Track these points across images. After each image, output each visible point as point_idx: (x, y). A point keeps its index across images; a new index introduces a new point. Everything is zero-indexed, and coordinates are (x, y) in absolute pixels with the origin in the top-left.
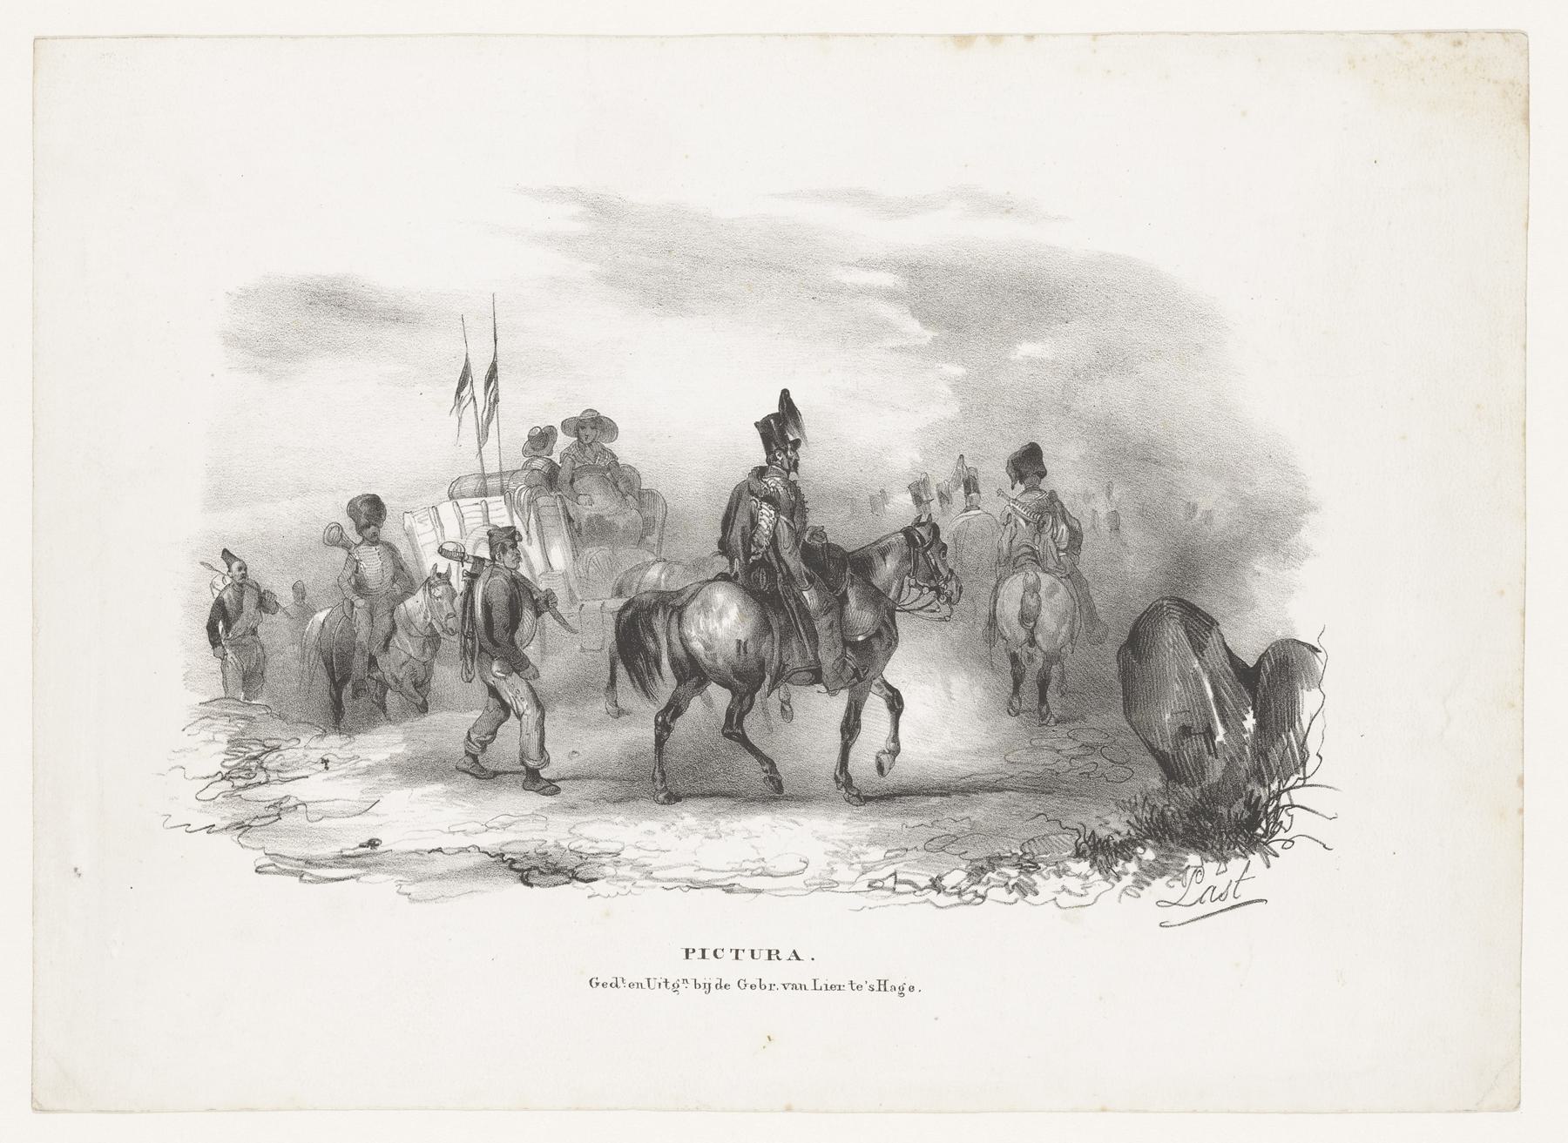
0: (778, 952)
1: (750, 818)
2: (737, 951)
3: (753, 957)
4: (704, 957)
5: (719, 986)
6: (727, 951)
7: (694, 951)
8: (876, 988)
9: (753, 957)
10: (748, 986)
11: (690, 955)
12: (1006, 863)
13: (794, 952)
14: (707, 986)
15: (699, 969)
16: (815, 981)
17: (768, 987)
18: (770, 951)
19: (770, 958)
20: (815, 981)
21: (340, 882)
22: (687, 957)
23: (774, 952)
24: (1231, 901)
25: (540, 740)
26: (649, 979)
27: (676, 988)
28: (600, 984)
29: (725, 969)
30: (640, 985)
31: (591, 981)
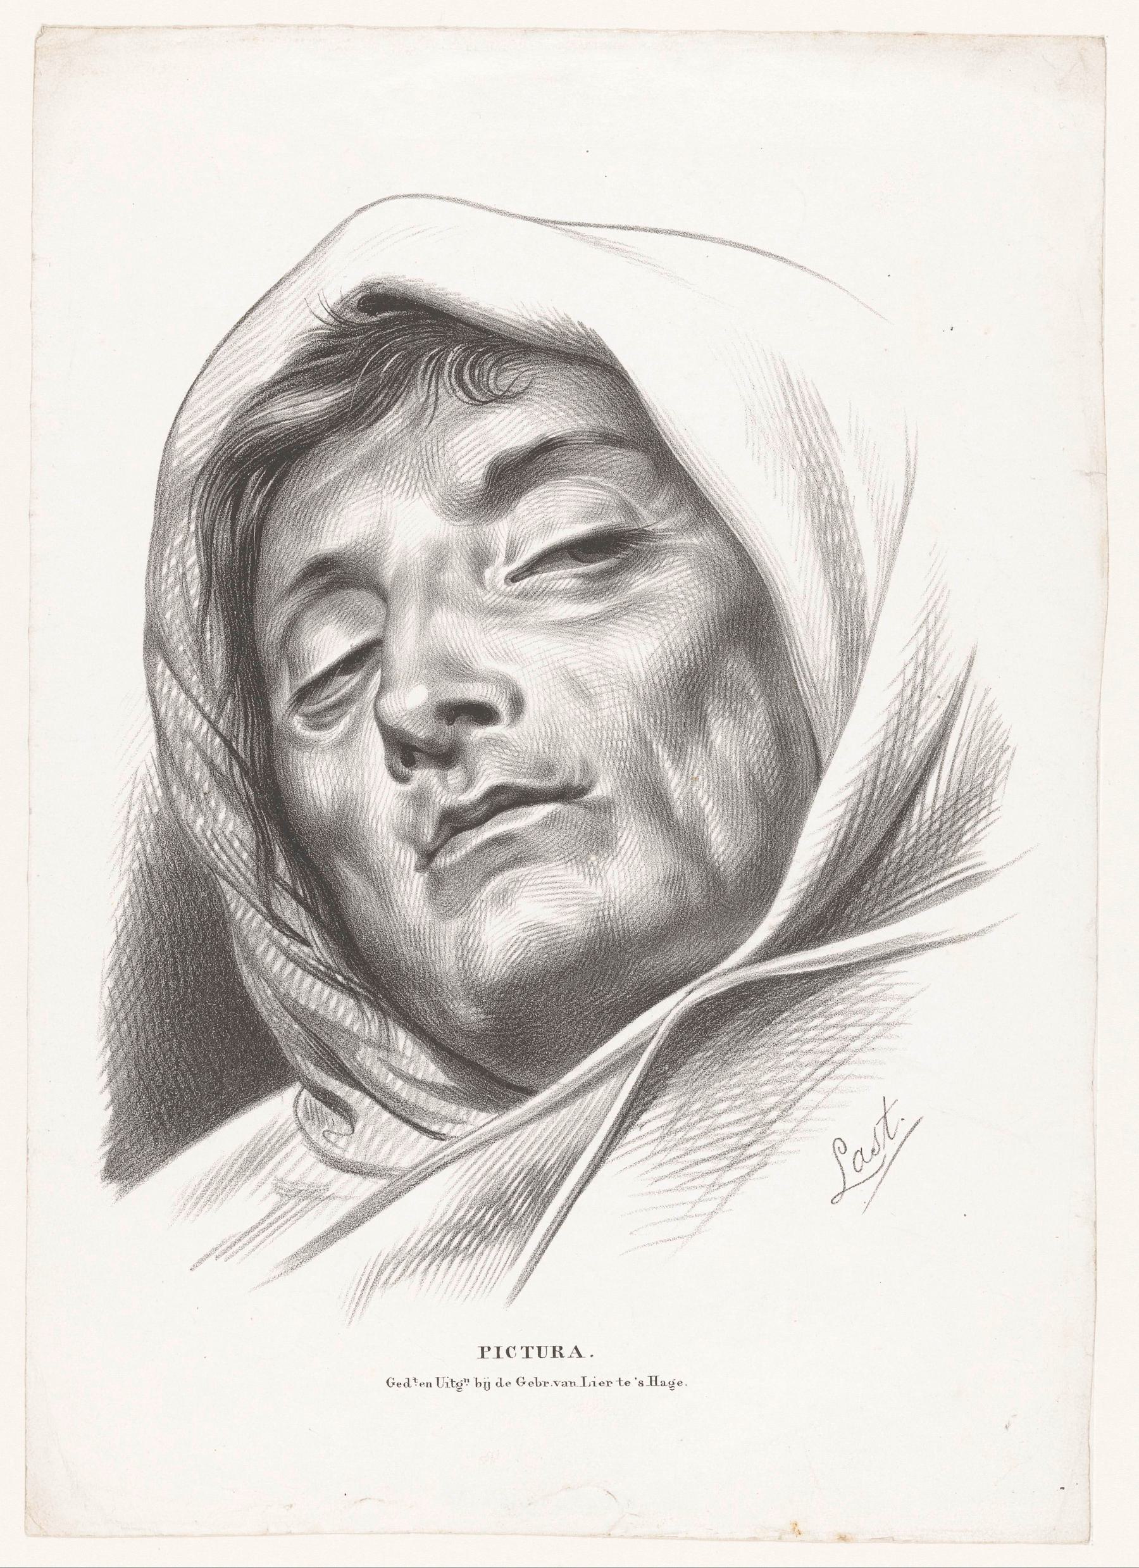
0: (561, 1348)
1: (385, 275)
2: (527, 1348)
4: (498, 1357)
7: (489, 1349)
10: (527, 1383)
13: (576, 1348)
15: (491, 1369)
16: (584, 1378)
17: (543, 1384)
18: (554, 1348)
19: (554, 1356)
20: (584, 1378)
22: (483, 1356)
23: (558, 1349)
26: (438, 1378)
28: (527, 1383)
29: (516, 1366)
30: (429, 1385)
31: (388, 1382)
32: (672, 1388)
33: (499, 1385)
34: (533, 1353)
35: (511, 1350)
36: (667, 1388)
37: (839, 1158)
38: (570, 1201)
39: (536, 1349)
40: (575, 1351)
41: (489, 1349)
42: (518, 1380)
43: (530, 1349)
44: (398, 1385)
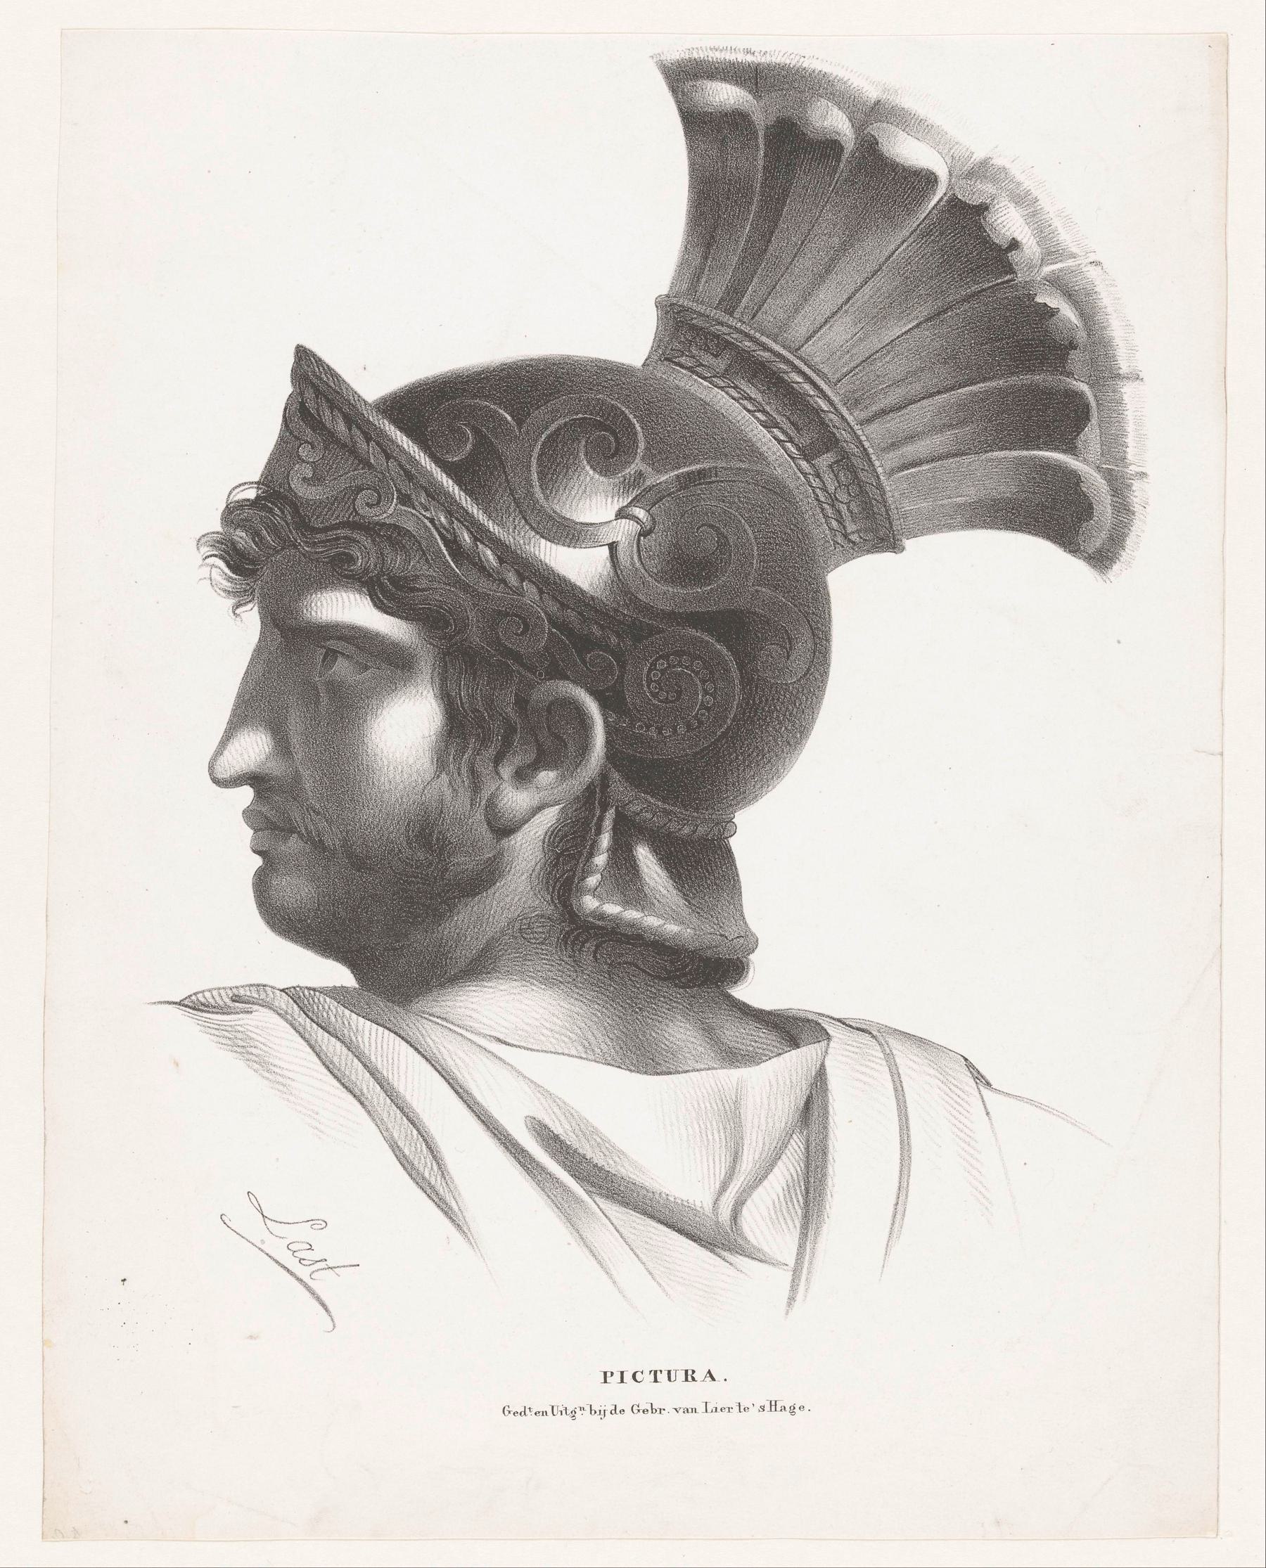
3: (669, 1379)
4: (622, 1381)
6: (646, 1372)
9: (669, 1379)
10: (641, 1411)
11: (608, 1379)
12: (659, 313)
13: (709, 1372)
14: (602, 1412)
15: (618, 1394)
18: (686, 1371)
21: (237, 484)
22: (605, 1382)
23: (690, 1373)
24: (303, 1272)
26: (553, 1407)
27: (573, 1415)
28: (641, 1411)
32: (792, 1412)
33: (523, 1413)
34: (662, 1377)
36: (787, 1413)
37: (982, 1093)
38: (440, 1069)
39: (665, 1373)
40: (708, 1375)
42: (504, 1408)
43: (659, 1372)
44: (644, 1411)
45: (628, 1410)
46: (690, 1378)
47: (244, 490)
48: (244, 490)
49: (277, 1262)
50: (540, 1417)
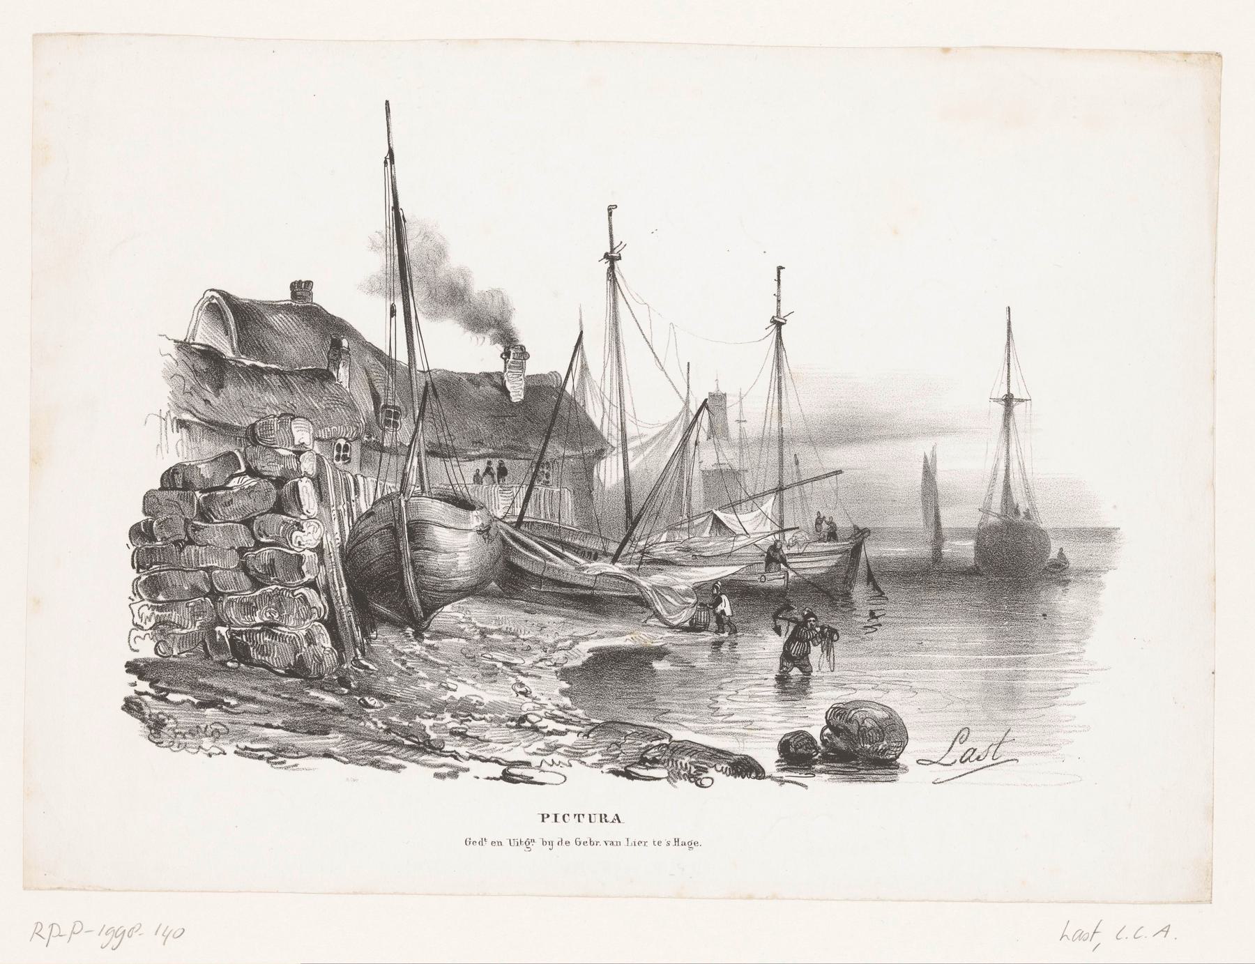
0: (606, 816)
2: (579, 815)
4: (556, 821)
5: (560, 843)
8: (581, 816)
11: (545, 819)
15: (552, 830)
18: (601, 815)
19: (601, 821)
22: (543, 821)
23: (603, 816)
25: (627, 508)
30: (500, 843)
35: (566, 816)
36: (524, 840)
39: (587, 817)
41: (548, 816)
45: (573, 842)
46: (603, 820)
47: (188, 332)
48: (188, 332)
49: (611, 228)
50: (497, 847)
